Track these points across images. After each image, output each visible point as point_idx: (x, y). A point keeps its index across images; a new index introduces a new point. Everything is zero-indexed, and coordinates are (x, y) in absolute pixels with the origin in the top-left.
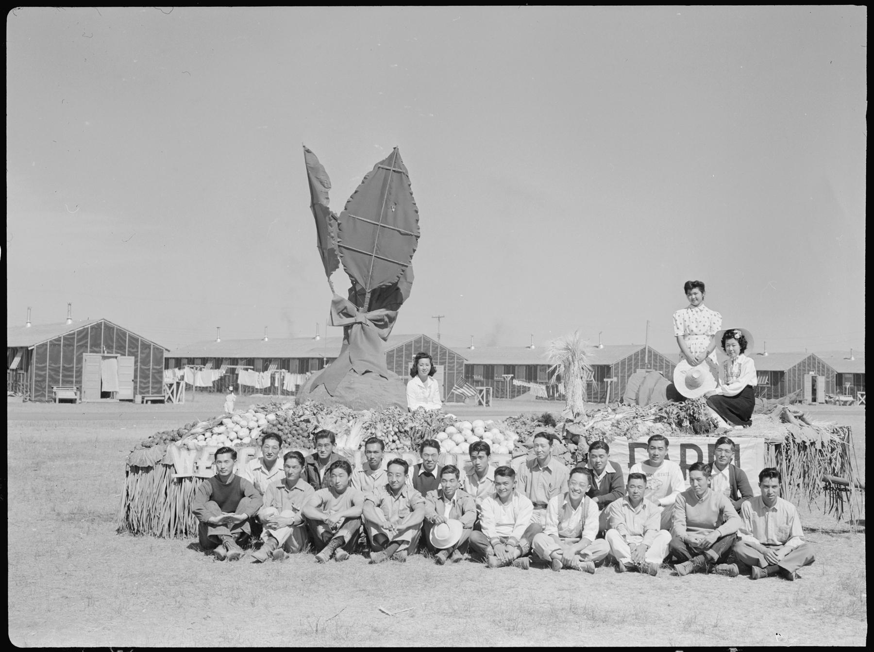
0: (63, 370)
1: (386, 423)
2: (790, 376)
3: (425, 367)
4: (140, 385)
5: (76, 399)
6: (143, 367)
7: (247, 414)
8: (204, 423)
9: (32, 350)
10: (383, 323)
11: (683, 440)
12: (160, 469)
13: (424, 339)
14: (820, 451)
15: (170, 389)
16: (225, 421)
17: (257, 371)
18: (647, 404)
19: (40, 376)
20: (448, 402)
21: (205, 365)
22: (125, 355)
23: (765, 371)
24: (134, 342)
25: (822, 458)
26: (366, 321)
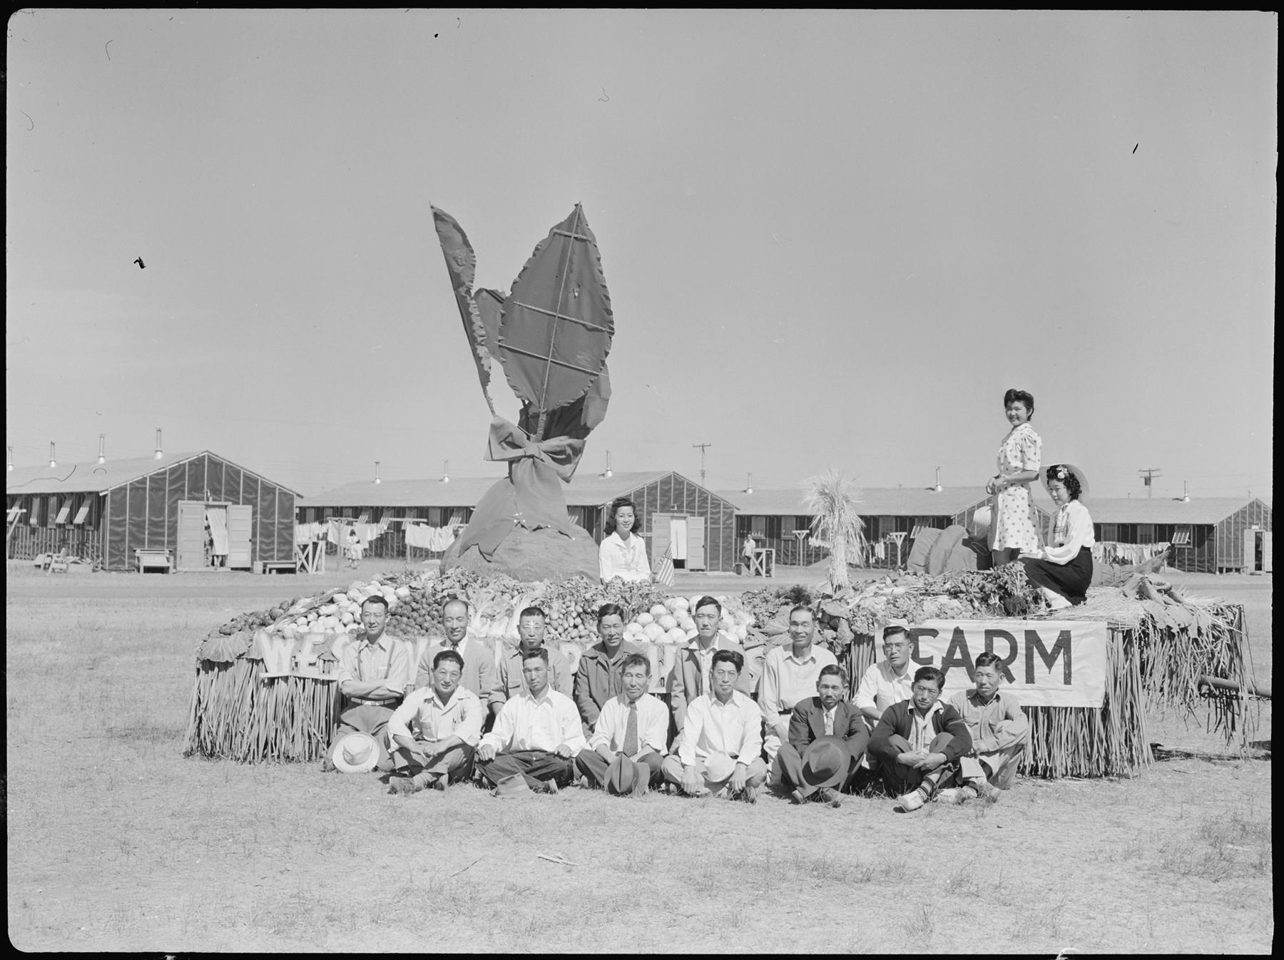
0: (149, 525)
1: (566, 600)
2: (1222, 532)
3: (627, 519)
4: (260, 547)
5: (168, 568)
6: (264, 520)
7: (368, 588)
8: (308, 600)
9: (105, 496)
10: (563, 456)
11: (989, 625)
12: (244, 665)
13: (675, 479)
14: (1195, 640)
15: (303, 553)
16: (336, 597)
17: (432, 526)
18: (942, 572)
19: (117, 534)
20: (711, 570)
21: (357, 517)
22: (238, 503)
23: (1185, 525)
24: (252, 484)
25: (1199, 651)
26: (540, 454)
